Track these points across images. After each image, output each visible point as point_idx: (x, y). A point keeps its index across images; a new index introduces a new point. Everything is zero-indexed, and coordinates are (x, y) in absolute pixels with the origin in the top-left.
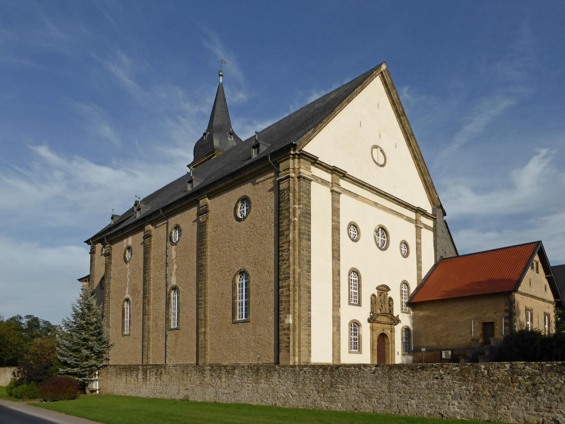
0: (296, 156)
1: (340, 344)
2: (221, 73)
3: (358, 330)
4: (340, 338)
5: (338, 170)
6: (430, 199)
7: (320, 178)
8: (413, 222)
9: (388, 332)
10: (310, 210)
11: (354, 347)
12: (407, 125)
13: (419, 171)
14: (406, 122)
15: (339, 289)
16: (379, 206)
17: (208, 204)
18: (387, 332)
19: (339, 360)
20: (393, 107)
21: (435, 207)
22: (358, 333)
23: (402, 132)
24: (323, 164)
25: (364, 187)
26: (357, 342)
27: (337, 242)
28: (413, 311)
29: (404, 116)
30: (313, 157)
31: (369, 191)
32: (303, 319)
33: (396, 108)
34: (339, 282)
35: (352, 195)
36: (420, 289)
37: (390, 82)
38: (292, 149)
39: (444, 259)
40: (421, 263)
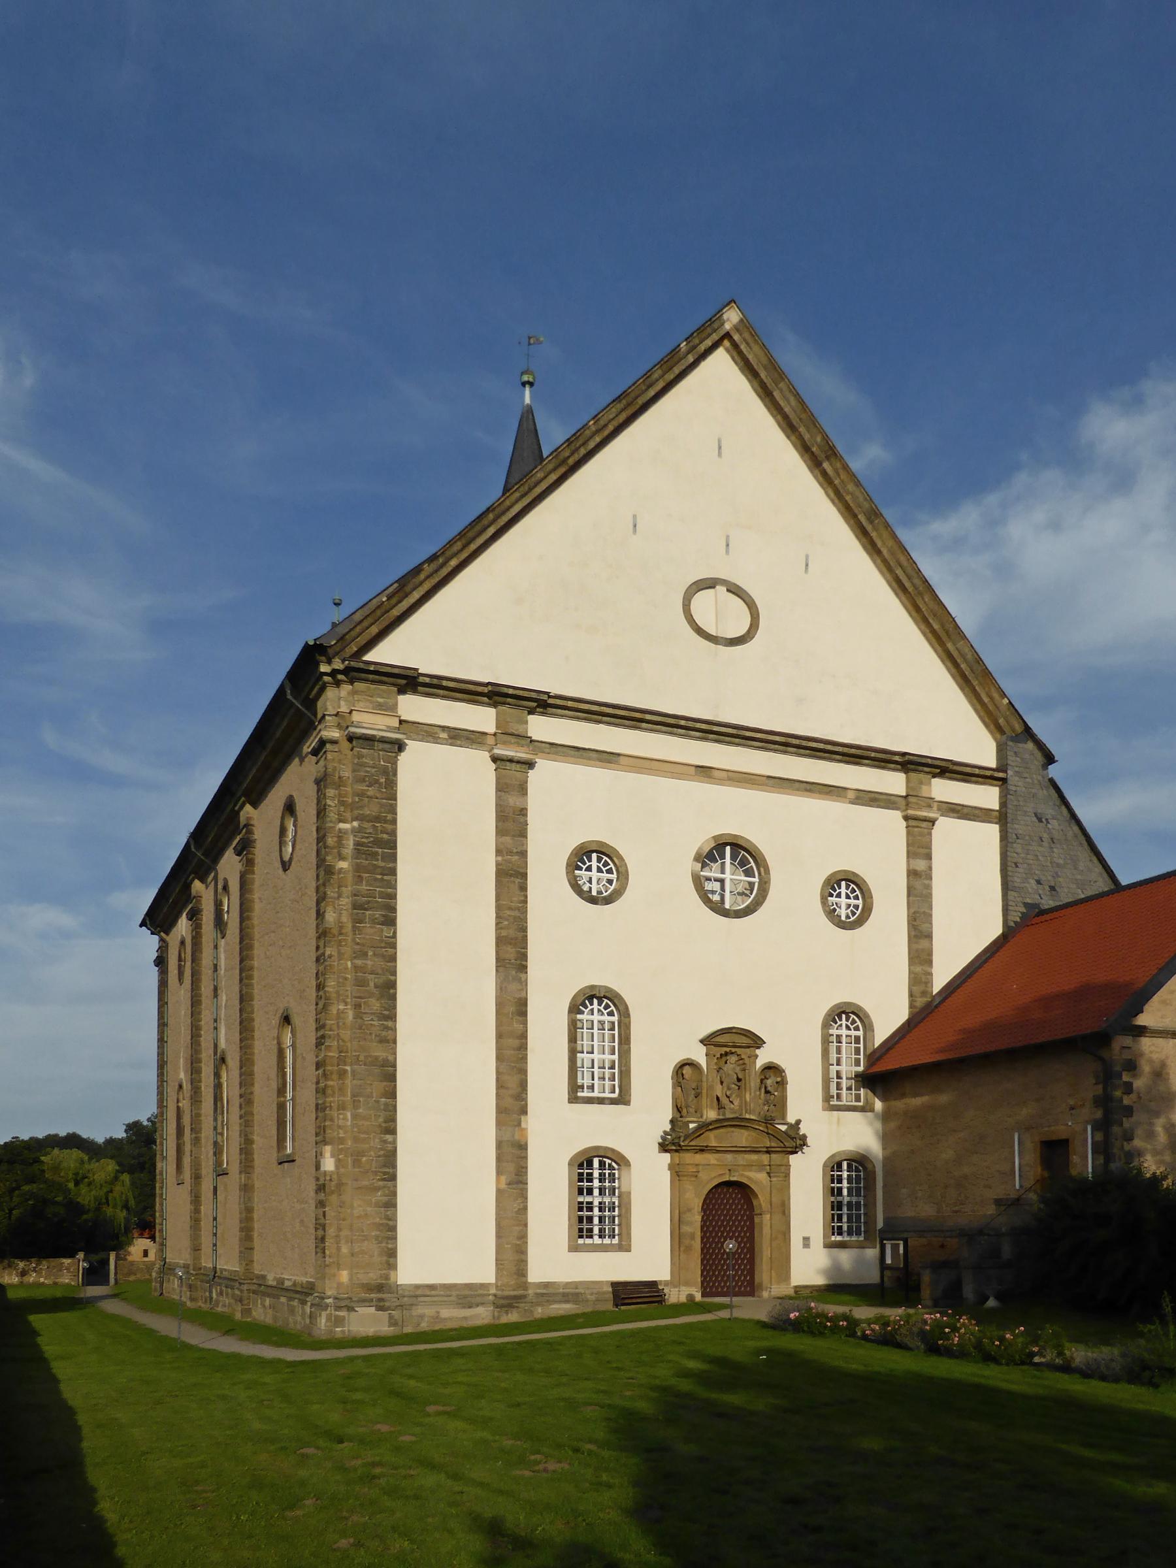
0: (340, 677)
1: (526, 1225)
2: (525, 378)
3: (618, 1179)
4: (525, 1208)
5: (511, 691)
6: (982, 714)
7: (444, 728)
8: (894, 803)
9: (757, 1178)
10: (393, 833)
11: (600, 1230)
12: (851, 487)
13: (923, 627)
14: (843, 476)
15: (524, 1059)
16: (716, 774)
17: (252, 823)
18: (749, 1178)
19: (521, 1269)
20: (793, 438)
21: (1004, 737)
22: (619, 1188)
23: (839, 510)
24: (445, 683)
25: (644, 725)
26: (616, 1213)
27: (516, 913)
28: (883, 1099)
29: (832, 459)
30: (396, 671)
31: (671, 733)
32: (364, 1159)
33: (800, 437)
34: (524, 1036)
35: (589, 759)
36: (916, 1026)
37: (764, 360)
38: (323, 658)
39: (1043, 912)
40: (929, 936)
